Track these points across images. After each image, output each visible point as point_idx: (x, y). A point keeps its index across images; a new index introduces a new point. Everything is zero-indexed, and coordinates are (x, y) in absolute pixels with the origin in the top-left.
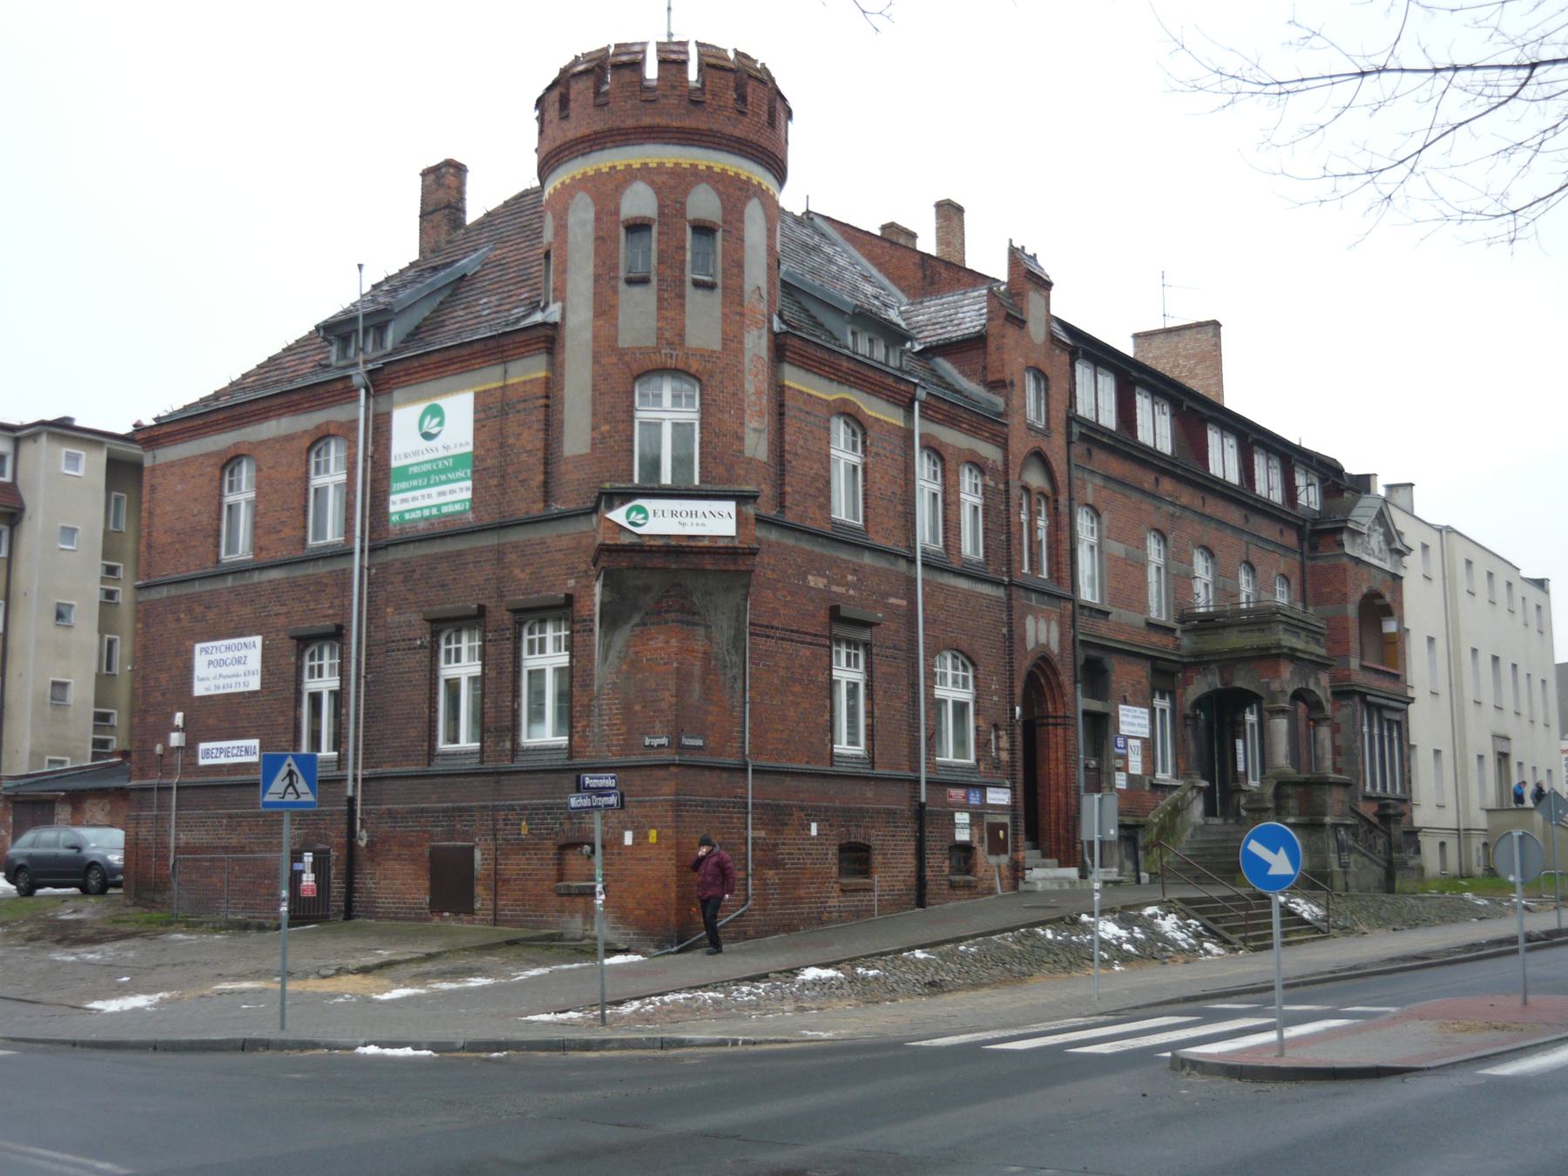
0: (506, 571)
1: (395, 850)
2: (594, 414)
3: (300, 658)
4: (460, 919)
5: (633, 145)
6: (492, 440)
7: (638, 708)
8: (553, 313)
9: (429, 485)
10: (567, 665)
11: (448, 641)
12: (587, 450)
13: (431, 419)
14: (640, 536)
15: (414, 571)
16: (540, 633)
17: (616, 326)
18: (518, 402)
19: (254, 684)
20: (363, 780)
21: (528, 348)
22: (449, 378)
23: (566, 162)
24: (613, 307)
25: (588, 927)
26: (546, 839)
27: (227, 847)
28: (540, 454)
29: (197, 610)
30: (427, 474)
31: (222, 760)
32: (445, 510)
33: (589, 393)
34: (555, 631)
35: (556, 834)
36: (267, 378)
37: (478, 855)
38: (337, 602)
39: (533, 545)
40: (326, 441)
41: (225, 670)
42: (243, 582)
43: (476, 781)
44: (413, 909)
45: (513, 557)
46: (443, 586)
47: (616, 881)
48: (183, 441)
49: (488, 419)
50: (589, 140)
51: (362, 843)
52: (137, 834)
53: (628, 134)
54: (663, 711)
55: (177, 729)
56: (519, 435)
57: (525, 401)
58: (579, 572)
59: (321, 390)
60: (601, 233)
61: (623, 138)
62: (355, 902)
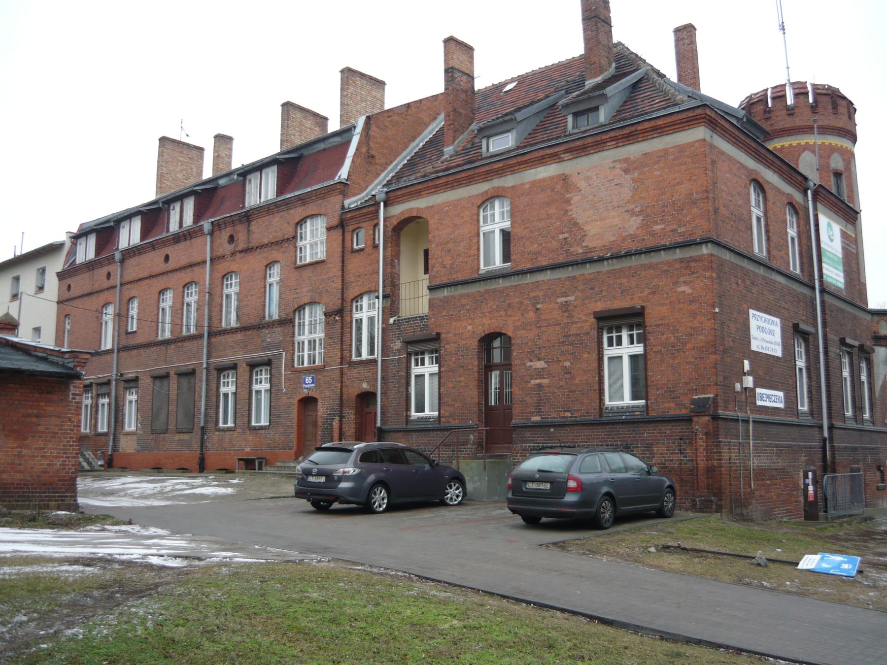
10: (642, 352)
11: (257, 375)
34: (608, 333)
40: (491, 201)
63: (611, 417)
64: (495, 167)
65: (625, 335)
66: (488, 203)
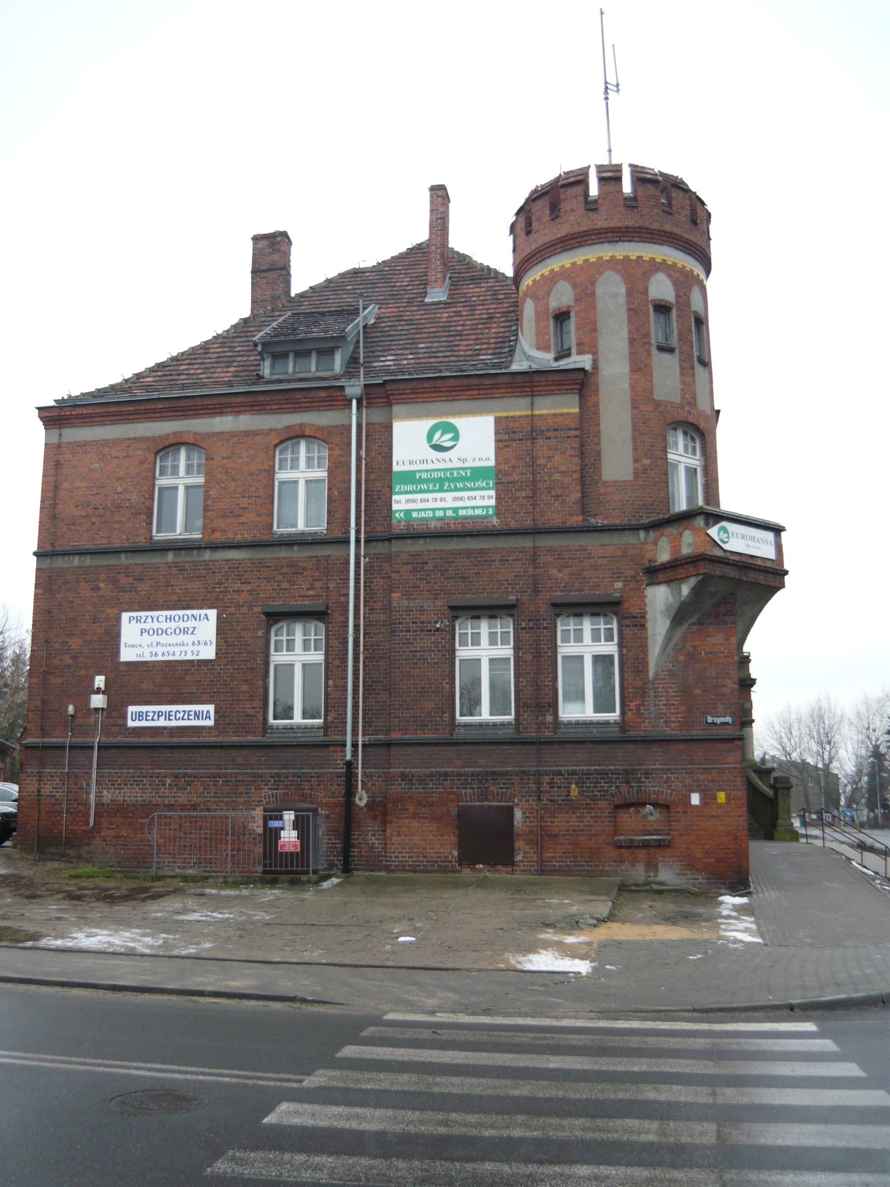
0: (542, 571)
1: (411, 809)
2: (635, 449)
3: (268, 632)
4: (498, 871)
5: (655, 243)
6: (518, 459)
7: (698, 691)
8: (584, 361)
9: (441, 490)
12: (629, 477)
13: (442, 434)
14: (725, 551)
15: (427, 563)
16: (288, 635)
17: (651, 381)
18: (548, 430)
19: (209, 653)
20: (363, 745)
21: (560, 387)
22: (461, 402)
23: (590, 244)
24: (648, 366)
25: (652, 874)
26: (600, 800)
27: (173, 805)
28: (576, 476)
29: (122, 581)
30: (441, 481)
31: (162, 723)
32: (462, 513)
33: (629, 432)
35: (613, 796)
36: (177, 380)
37: (518, 814)
38: (318, 584)
39: (571, 550)
41: (163, 639)
42: (189, 559)
43: (510, 750)
44: (437, 862)
45: (549, 559)
46: (464, 578)
47: (681, 835)
48: (102, 424)
49: (513, 440)
50: (620, 232)
51: (362, 803)
52: (39, 791)
53: (653, 234)
54: (725, 695)
55: (98, 691)
56: (550, 457)
57: (555, 430)
58: (625, 577)
59: (298, 395)
60: (632, 306)
61: (648, 236)
62: (352, 856)
63: (572, 734)
64: (125, 409)
65: (299, 638)
66: (289, 443)
